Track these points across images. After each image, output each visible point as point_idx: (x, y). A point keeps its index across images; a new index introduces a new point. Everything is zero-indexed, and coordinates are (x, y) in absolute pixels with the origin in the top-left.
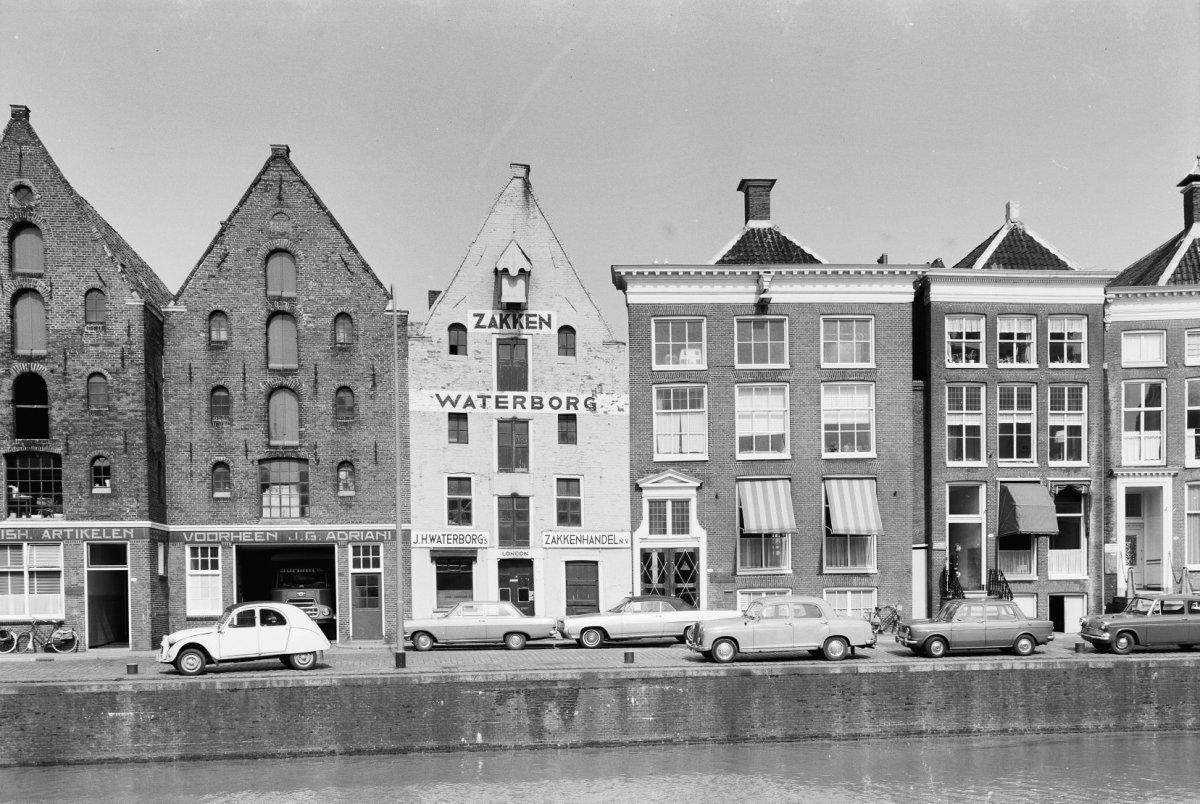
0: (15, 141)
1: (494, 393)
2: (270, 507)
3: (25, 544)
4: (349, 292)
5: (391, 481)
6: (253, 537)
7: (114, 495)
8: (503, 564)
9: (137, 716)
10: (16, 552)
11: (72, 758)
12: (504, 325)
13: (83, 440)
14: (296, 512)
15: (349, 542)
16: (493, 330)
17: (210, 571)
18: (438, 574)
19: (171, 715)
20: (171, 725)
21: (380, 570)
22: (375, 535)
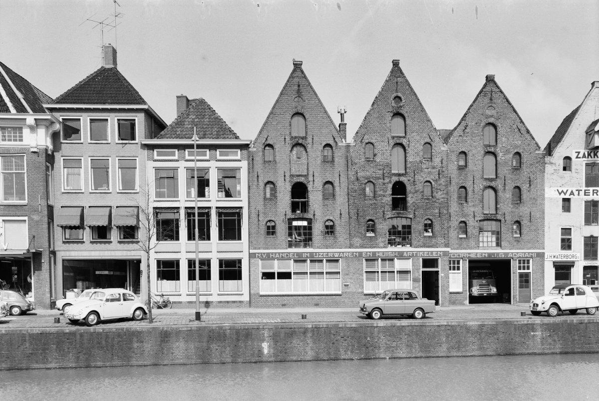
0: (395, 76)
1: (584, 188)
2: (483, 242)
3: (396, 258)
4: (520, 142)
5: (536, 230)
6: (477, 255)
7: (434, 236)
8: (585, 268)
9: (542, 334)
10: (391, 262)
11: (517, 352)
12: (589, 157)
13: (421, 211)
14: (494, 244)
15: (518, 258)
16: (584, 159)
17: (456, 271)
18: (556, 273)
19: (556, 334)
20: (556, 338)
21: (530, 271)
22: (407, 254)
